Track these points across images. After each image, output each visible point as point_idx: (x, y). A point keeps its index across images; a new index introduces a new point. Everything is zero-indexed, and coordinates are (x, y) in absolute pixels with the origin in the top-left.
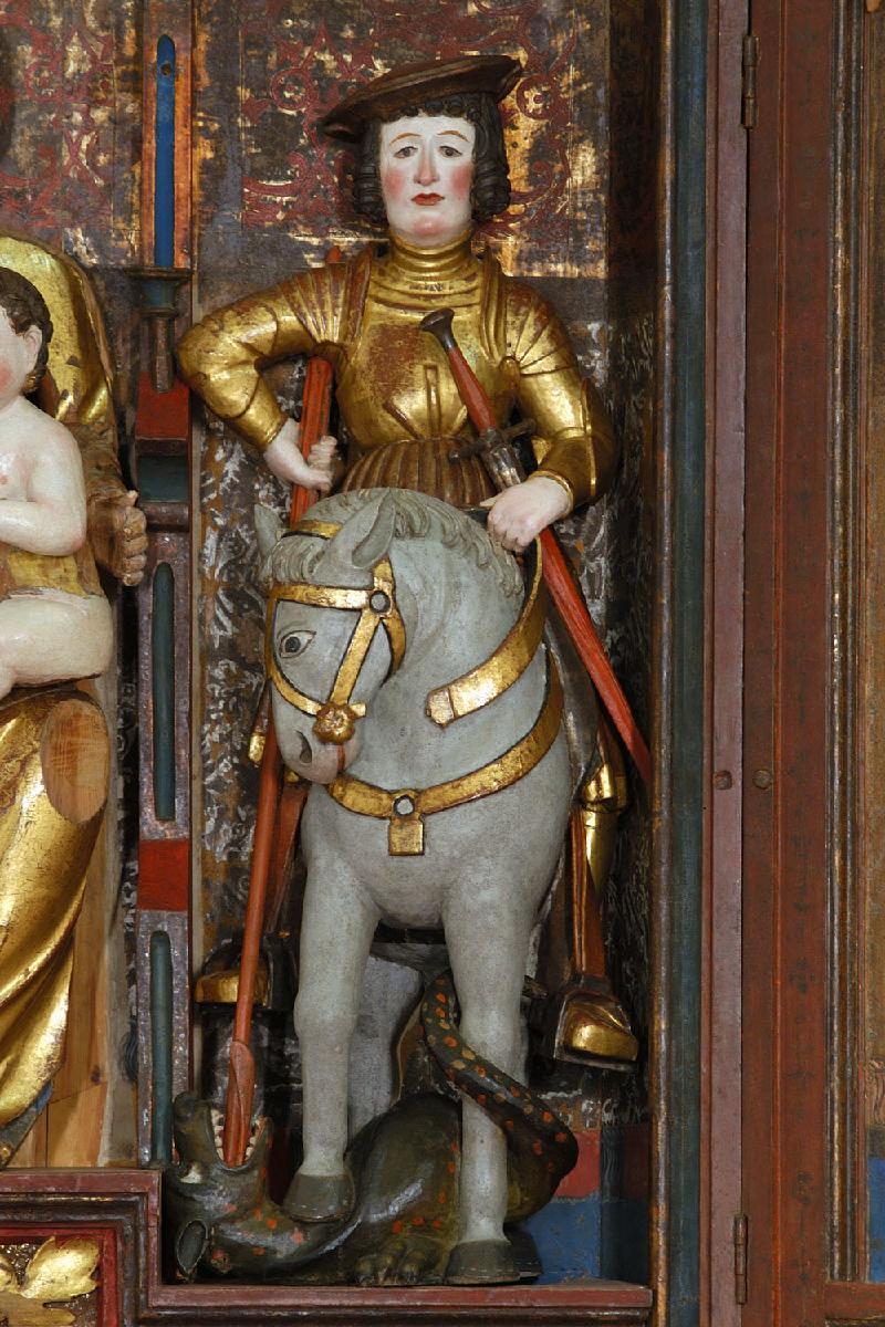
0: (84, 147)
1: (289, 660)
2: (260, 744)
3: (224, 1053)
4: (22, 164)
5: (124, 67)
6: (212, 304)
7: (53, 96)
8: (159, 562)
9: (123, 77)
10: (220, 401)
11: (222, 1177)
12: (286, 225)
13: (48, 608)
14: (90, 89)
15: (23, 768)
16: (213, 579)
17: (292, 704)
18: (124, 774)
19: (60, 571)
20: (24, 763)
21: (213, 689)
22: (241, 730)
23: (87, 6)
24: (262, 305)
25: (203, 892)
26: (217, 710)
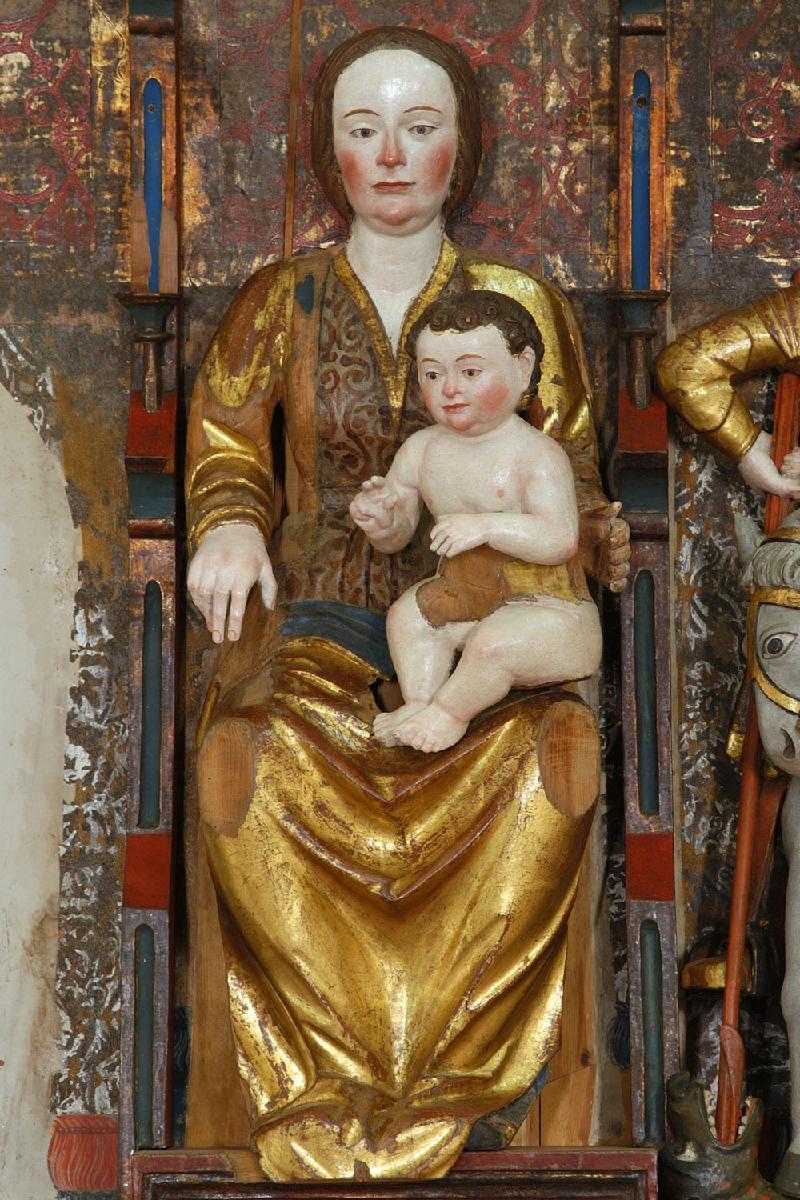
0: (562, 177)
1: (771, 660)
2: (738, 741)
3: (706, 1036)
4: (504, 195)
5: (600, 101)
6: (684, 324)
7: (533, 130)
8: (640, 569)
9: (599, 111)
10: (698, 416)
11: (717, 1155)
12: (755, 247)
13: (544, 613)
14: (569, 123)
15: (521, 766)
16: (688, 585)
17: (776, 704)
18: (607, 771)
19: (554, 578)
20: (522, 761)
21: (690, 690)
22: (717, 728)
23: (565, 45)
24: (737, 323)
25: (684, 882)
26: (693, 711)
